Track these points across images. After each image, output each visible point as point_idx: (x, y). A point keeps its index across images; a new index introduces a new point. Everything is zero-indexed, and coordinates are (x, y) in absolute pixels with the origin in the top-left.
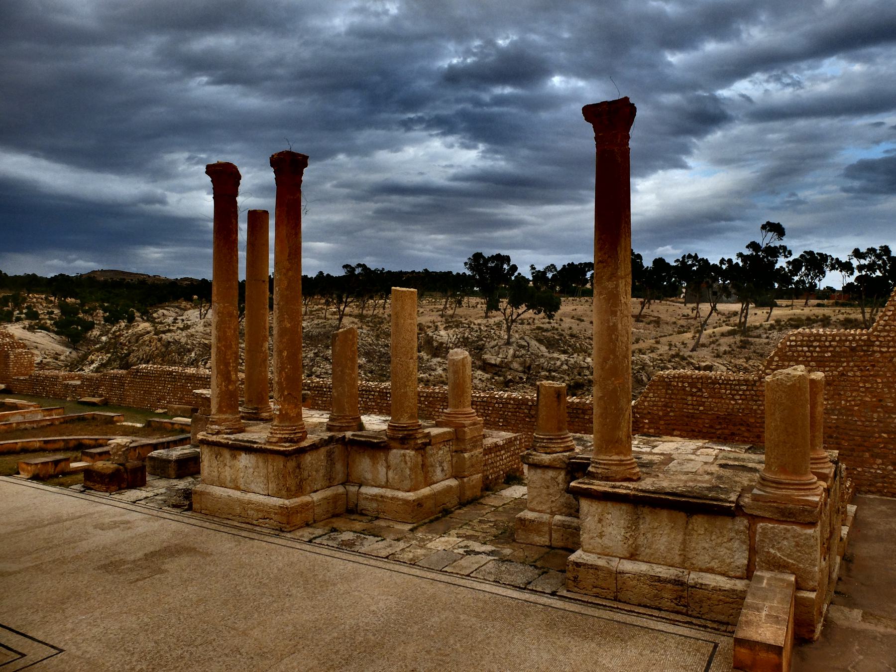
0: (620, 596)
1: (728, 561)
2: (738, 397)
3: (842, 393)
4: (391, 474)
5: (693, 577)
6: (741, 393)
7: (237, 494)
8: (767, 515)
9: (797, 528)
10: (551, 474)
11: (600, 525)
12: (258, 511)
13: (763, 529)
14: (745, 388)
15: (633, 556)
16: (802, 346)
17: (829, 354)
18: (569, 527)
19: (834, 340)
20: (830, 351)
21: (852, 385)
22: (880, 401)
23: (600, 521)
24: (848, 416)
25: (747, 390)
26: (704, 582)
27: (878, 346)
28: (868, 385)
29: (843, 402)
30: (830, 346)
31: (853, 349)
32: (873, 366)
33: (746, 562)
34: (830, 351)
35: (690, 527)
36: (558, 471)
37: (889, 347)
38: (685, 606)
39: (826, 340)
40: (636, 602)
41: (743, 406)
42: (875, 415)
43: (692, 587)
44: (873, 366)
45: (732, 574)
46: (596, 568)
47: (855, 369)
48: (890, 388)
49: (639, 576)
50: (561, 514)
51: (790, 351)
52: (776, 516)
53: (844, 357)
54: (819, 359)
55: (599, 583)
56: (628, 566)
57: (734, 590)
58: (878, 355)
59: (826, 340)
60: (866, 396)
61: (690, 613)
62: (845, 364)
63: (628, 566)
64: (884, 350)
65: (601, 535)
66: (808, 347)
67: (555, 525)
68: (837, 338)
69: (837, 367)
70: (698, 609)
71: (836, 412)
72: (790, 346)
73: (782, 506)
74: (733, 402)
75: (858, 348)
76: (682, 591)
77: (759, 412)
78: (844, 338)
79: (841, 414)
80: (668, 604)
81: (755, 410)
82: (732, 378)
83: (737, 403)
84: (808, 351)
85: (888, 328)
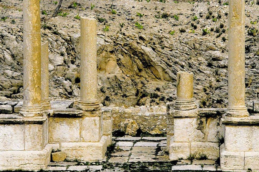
12: (19, 160)
36: (192, 119)
56: (248, 154)
63: (248, 154)
65: (236, 142)
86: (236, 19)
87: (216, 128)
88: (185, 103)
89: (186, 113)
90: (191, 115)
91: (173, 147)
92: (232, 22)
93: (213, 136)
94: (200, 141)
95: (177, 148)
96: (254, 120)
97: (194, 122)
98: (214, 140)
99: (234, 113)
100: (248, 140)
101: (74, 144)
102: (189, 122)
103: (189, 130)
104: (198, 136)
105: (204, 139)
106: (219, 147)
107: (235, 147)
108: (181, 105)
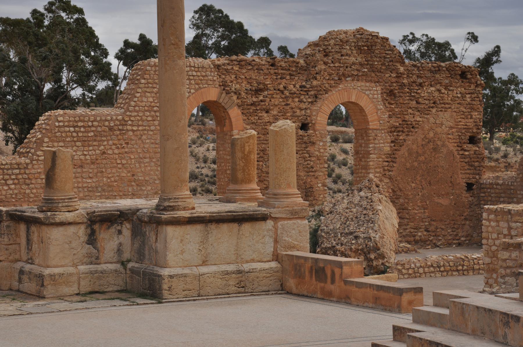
0: (202, 292)
1: (262, 251)
2: (10, 182)
3: (104, 170)
5: (246, 267)
6: (13, 177)
8: (284, 216)
9: (299, 221)
10: (72, 229)
11: (181, 245)
13: (282, 226)
14: (17, 171)
15: (204, 263)
16: (68, 126)
17: (92, 134)
18: (96, 272)
19: (95, 120)
20: (93, 131)
21: (112, 163)
22: (133, 175)
23: (182, 241)
24: (109, 191)
25: (20, 174)
26: (254, 267)
27: (130, 125)
28: (124, 162)
29: (105, 179)
30: (93, 126)
31: (111, 129)
32: (127, 143)
33: (272, 250)
34: (93, 131)
35: (241, 233)
36: (79, 226)
37: (139, 126)
38: (243, 287)
39: (89, 121)
40: (212, 293)
41: (16, 191)
42: (130, 189)
43: (247, 272)
44: (127, 143)
45: (265, 260)
46: (185, 276)
47: (114, 147)
48: (140, 163)
49: (214, 274)
50: (82, 264)
51: (59, 131)
52: (288, 216)
53: (104, 136)
54: (84, 139)
55: (188, 287)
56: (204, 270)
57: (271, 268)
58: (131, 133)
59: (89, 121)
60: (123, 172)
61: (246, 290)
62: (105, 143)
63: (204, 270)
64: (135, 128)
65: (182, 252)
66: (74, 127)
67: (83, 273)
68: (98, 119)
69: (99, 146)
70: (251, 287)
71: (100, 189)
72: (59, 127)
73: (291, 209)
74: (6, 188)
75: (116, 128)
76: (242, 277)
77: (32, 195)
78: (103, 118)
79: (104, 190)
80: (233, 288)
81: (28, 194)
82: (4, 163)
83: (10, 189)
84: (74, 132)
85: (137, 108)
86: (175, 48)
87: (116, 239)
88: (66, 201)
89: (69, 216)
90: (78, 220)
91: (51, 276)
92: (168, 53)
93: (112, 254)
94: (91, 263)
95: (57, 277)
96: (213, 213)
97: (82, 231)
98: (114, 258)
99: (180, 204)
100: (202, 247)
102: (74, 233)
103: (74, 245)
104: (89, 255)
105: (96, 260)
106: (7, 288)
107: (181, 260)
108: (59, 202)
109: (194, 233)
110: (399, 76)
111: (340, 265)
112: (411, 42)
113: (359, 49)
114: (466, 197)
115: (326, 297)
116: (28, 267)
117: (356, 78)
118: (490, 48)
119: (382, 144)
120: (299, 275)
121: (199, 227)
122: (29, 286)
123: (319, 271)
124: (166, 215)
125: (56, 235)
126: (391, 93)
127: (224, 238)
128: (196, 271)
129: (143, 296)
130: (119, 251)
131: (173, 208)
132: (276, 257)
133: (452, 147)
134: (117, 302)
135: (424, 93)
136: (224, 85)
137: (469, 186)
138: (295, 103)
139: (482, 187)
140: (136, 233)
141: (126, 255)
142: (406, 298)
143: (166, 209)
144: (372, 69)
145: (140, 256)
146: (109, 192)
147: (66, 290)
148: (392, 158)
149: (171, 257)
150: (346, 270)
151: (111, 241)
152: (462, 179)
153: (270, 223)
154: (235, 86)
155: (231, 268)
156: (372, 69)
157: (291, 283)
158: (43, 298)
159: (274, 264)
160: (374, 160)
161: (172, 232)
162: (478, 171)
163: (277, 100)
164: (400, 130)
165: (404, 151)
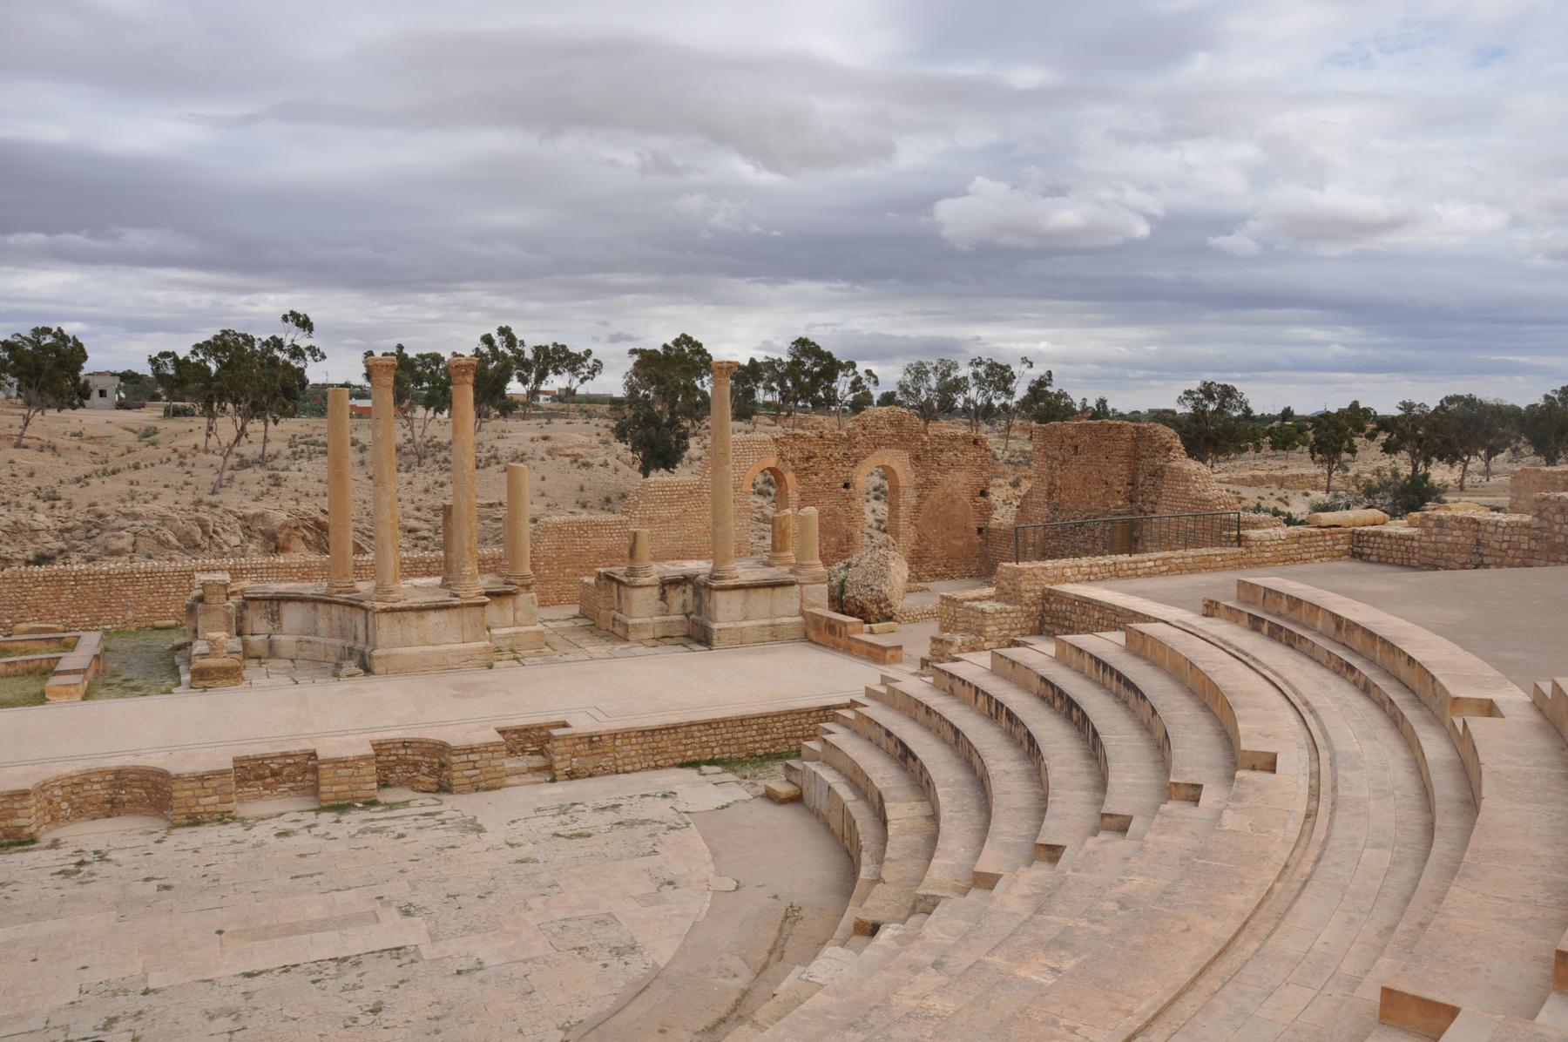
4: (519, 615)
5: (778, 621)
7: (430, 649)
15: (746, 619)
49: (752, 628)
56: (745, 624)
63: (745, 624)
89: (646, 581)
97: (656, 592)
101: (507, 631)
105: (666, 612)
109: (737, 596)
110: (924, 444)
111: (845, 624)
112: (978, 364)
113: (891, 423)
114: (977, 539)
115: (835, 647)
116: (618, 616)
117: (889, 446)
118: (1043, 372)
119: (909, 498)
120: (818, 629)
121: (741, 592)
122: (619, 630)
123: (832, 627)
124: (715, 584)
125: (637, 593)
126: (917, 458)
127: (760, 599)
128: (739, 625)
129: (699, 642)
130: (684, 606)
131: (721, 578)
132: (802, 613)
133: (966, 499)
134: (680, 648)
135: (944, 457)
136: (781, 454)
137: (980, 530)
138: (838, 467)
139: (989, 531)
140: (696, 593)
141: (689, 609)
142: (889, 653)
143: (716, 578)
144: (902, 438)
145: (699, 610)
146: (684, 555)
147: (645, 635)
148: (917, 509)
149: (719, 615)
150: (850, 628)
151: (677, 598)
152: (973, 525)
153: (797, 587)
154: (790, 455)
155: (766, 622)
156: (902, 438)
157: (812, 634)
158: (627, 640)
159: (799, 619)
160: (903, 511)
161: (720, 597)
162: (987, 518)
163: (824, 465)
164: (925, 486)
165: (927, 504)
